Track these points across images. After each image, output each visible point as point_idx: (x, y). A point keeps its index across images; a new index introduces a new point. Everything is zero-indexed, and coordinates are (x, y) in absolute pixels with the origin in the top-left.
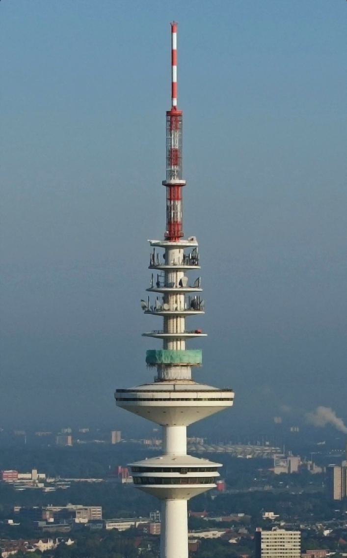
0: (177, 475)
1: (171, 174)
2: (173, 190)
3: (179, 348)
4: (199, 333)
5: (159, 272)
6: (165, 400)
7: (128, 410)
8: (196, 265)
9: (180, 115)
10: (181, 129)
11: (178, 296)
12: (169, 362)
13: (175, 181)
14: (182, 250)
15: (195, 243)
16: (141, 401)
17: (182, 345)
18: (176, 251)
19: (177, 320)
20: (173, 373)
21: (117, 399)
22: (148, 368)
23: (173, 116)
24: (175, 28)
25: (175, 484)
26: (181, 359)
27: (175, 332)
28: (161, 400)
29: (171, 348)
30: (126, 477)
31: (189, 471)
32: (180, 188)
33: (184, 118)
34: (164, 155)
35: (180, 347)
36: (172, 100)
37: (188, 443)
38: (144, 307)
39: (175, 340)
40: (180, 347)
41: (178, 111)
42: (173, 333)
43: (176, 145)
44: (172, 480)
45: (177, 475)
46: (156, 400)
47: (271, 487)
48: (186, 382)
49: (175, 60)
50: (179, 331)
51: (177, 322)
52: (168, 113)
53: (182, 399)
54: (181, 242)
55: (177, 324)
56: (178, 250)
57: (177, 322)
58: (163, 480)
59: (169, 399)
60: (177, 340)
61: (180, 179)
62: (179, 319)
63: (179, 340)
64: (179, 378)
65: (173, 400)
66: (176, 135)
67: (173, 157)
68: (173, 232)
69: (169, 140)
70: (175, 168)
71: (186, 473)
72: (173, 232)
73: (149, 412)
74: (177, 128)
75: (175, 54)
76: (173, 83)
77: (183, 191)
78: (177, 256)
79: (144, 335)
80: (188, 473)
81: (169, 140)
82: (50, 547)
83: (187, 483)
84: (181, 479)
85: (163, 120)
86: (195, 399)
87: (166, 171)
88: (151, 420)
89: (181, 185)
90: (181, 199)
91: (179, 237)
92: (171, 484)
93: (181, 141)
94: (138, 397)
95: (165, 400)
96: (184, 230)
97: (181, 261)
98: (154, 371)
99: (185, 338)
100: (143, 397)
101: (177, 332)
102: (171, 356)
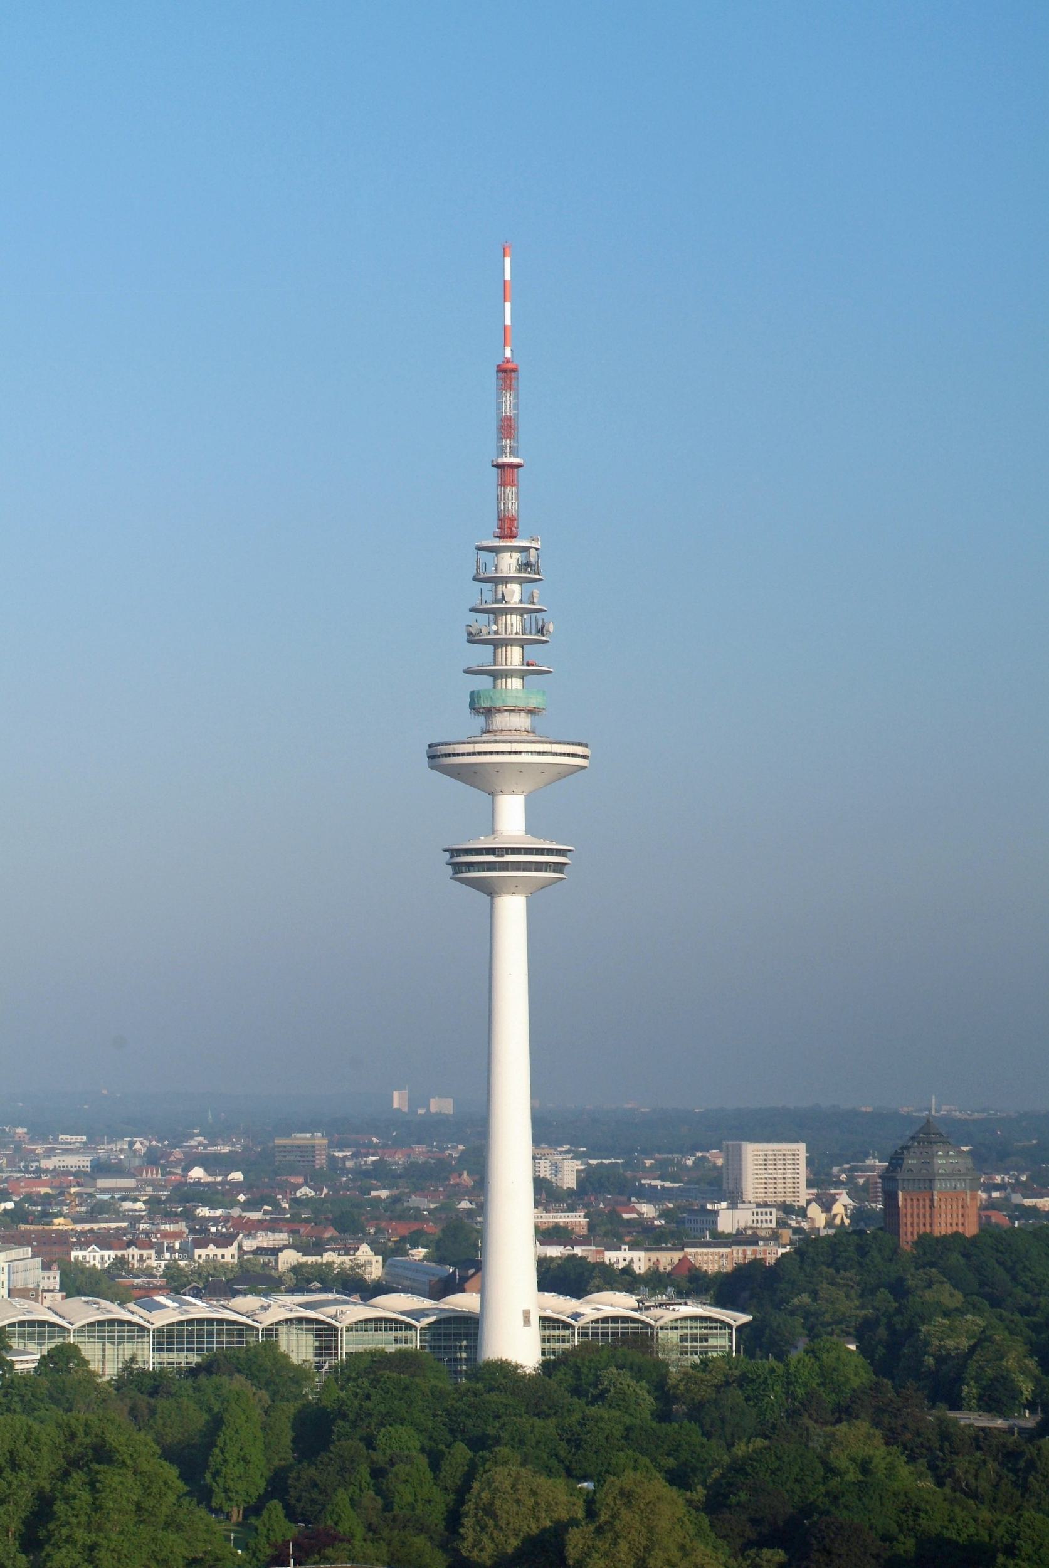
1: (502, 451)
3: (504, 687)
4: (533, 665)
5: (489, 586)
6: (469, 754)
7: (436, 770)
8: (529, 573)
9: (515, 370)
10: (516, 390)
11: (509, 616)
14: (516, 555)
17: (515, 683)
18: (506, 555)
20: (502, 721)
21: (429, 757)
22: (476, 717)
23: (506, 373)
24: (507, 250)
27: (504, 664)
28: (463, 754)
31: (507, 854)
38: (470, 634)
39: (504, 676)
41: (510, 365)
43: (508, 410)
44: (528, 865)
46: (459, 755)
48: (523, 733)
49: (508, 342)
50: (509, 664)
52: (501, 369)
54: (515, 543)
59: (474, 754)
60: (506, 677)
61: (516, 456)
62: (509, 648)
63: (504, 676)
64: (506, 729)
65: (479, 753)
66: (509, 398)
67: (507, 428)
68: (507, 528)
69: (499, 408)
71: (502, 856)
72: (507, 528)
78: (509, 563)
79: (468, 671)
81: (499, 408)
83: (518, 870)
86: (510, 753)
88: (476, 787)
89: (519, 466)
90: (515, 485)
91: (513, 537)
92: (508, 871)
95: (469, 754)
96: (521, 527)
97: (513, 569)
98: (481, 720)
99: (520, 612)
101: (506, 665)
102: (491, 698)
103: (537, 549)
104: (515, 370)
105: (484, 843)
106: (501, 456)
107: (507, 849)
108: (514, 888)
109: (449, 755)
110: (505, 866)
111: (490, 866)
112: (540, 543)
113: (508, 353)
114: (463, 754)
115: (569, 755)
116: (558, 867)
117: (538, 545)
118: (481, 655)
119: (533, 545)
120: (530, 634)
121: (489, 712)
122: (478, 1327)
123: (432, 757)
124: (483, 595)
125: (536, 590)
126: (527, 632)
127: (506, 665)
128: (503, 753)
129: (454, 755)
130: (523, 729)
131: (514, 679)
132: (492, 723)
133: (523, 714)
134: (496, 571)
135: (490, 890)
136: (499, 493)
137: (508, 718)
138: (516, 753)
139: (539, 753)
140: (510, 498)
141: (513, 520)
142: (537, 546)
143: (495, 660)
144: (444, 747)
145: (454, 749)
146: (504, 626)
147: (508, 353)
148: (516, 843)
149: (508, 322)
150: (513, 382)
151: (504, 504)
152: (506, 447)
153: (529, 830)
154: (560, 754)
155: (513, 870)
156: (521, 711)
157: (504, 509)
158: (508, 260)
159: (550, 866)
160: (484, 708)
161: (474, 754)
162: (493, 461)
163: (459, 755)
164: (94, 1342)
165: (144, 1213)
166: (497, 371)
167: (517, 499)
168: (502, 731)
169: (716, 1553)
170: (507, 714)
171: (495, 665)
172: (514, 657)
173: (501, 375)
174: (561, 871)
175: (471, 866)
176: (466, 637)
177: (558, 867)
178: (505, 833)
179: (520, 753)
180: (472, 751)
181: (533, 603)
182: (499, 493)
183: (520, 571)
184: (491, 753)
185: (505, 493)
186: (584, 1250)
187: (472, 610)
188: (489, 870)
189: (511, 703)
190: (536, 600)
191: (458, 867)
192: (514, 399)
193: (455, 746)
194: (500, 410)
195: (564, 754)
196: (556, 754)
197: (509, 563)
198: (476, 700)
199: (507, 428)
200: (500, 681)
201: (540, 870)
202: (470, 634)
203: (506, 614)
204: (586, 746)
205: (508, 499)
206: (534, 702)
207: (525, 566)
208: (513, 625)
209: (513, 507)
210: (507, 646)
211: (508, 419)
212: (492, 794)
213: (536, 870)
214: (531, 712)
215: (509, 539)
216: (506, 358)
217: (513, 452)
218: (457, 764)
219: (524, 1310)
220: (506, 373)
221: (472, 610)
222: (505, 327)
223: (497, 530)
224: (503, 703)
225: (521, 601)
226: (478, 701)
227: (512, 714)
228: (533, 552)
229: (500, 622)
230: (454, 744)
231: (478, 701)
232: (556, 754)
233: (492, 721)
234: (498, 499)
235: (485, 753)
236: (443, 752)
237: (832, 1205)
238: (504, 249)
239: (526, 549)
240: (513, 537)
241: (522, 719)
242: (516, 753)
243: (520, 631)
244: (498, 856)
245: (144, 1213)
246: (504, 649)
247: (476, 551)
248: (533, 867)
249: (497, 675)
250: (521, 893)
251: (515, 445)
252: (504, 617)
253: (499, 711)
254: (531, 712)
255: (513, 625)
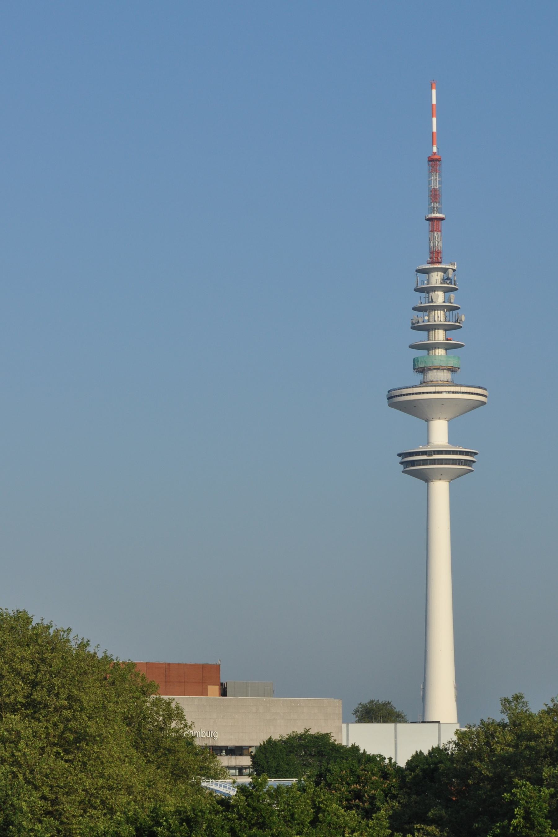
0: (425, 457)
1: (432, 211)
3: (434, 354)
4: (451, 340)
6: (410, 394)
12: (423, 366)
16: (393, 398)
17: (440, 352)
19: (435, 332)
20: (433, 375)
24: (434, 85)
25: (430, 464)
26: (432, 362)
27: (433, 340)
28: (407, 395)
29: (431, 354)
31: (435, 454)
32: (440, 222)
33: (443, 162)
34: (426, 196)
35: (435, 353)
36: (432, 147)
40: (435, 353)
41: (436, 157)
42: (432, 340)
45: (425, 457)
46: (404, 395)
49: (435, 142)
51: (435, 333)
53: (427, 393)
55: (435, 335)
56: (436, 273)
57: (435, 333)
58: (429, 462)
59: (413, 394)
63: (434, 348)
65: (416, 394)
66: (436, 177)
67: (434, 195)
70: (434, 205)
71: (431, 455)
73: (415, 406)
74: (436, 171)
79: (413, 347)
80: (434, 456)
83: (442, 464)
84: (444, 460)
86: (435, 393)
87: (429, 208)
89: (442, 219)
90: (440, 231)
93: (440, 182)
94: (392, 395)
95: (410, 394)
96: (444, 256)
97: (439, 282)
100: (405, 393)
102: (425, 361)
103: (454, 270)
104: (439, 160)
105: (421, 449)
106: (431, 213)
107: (434, 451)
108: (440, 476)
109: (399, 396)
110: (433, 462)
111: (425, 462)
112: (456, 266)
113: (435, 149)
114: (407, 395)
115: (472, 393)
117: (455, 267)
118: (420, 337)
119: (451, 267)
120: (449, 321)
121: (423, 371)
122: (381, 722)
123: (389, 398)
124: (420, 300)
125: (452, 295)
126: (447, 320)
127: (435, 340)
128: (431, 393)
129: (401, 395)
130: (446, 380)
131: (439, 350)
132: (427, 377)
133: (445, 371)
134: (428, 283)
135: (426, 478)
136: (430, 236)
137: (436, 374)
138: (438, 392)
139: (453, 392)
140: (437, 239)
141: (438, 253)
142: (453, 268)
143: (428, 339)
144: (396, 391)
145: (401, 392)
146: (433, 317)
147: (435, 149)
148: (442, 448)
150: (438, 168)
151: (433, 242)
152: (434, 208)
153: (450, 442)
154: (466, 393)
155: (438, 464)
156: (443, 369)
157: (433, 245)
158: (434, 91)
159: (462, 462)
160: (421, 368)
161: (413, 394)
162: (426, 217)
163: (404, 395)
166: (429, 161)
167: (441, 240)
168: (432, 381)
169: (320, 761)
170: (435, 371)
171: (428, 341)
172: (440, 336)
173: (431, 163)
174: (469, 466)
175: (413, 463)
176: (410, 325)
178: (435, 444)
179: (441, 392)
180: (412, 392)
181: (451, 302)
182: (430, 236)
183: (442, 283)
184: (423, 393)
185: (433, 236)
187: (415, 309)
188: (424, 465)
189: (437, 363)
190: (452, 301)
191: (406, 464)
192: (439, 178)
193: (401, 390)
194: (430, 185)
195: (472, 393)
196: (463, 393)
197: (436, 279)
198: (416, 363)
199: (434, 195)
200: (431, 351)
201: (456, 464)
202: (413, 324)
203: (435, 310)
204: (485, 389)
205: (435, 240)
206: (452, 363)
207: (446, 280)
208: (439, 317)
209: (439, 244)
210: (435, 329)
211: (435, 190)
212: (427, 420)
213: (453, 464)
214: (452, 370)
215: (438, 264)
216: (434, 152)
218: (402, 401)
220: (434, 161)
221: (415, 309)
222: (433, 133)
223: (429, 259)
224: (432, 364)
225: (444, 302)
226: (417, 364)
227: (439, 371)
228: (450, 271)
229: (431, 315)
230: (401, 389)
231: (417, 364)
232: (463, 393)
233: (426, 376)
234: (429, 240)
235: (420, 393)
236: (395, 395)
238: (432, 84)
239: (445, 271)
240: (440, 263)
241: (445, 374)
242: (438, 392)
243: (444, 320)
244: (429, 456)
246: (433, 331)
247: (416, 273)
248: (451, 462)
249: (429, 347)
250: (444, 479)
251: (440, 206)
252: (433, 312)
253: (430, 369)
254: (452, 370)
255: (439, 317)
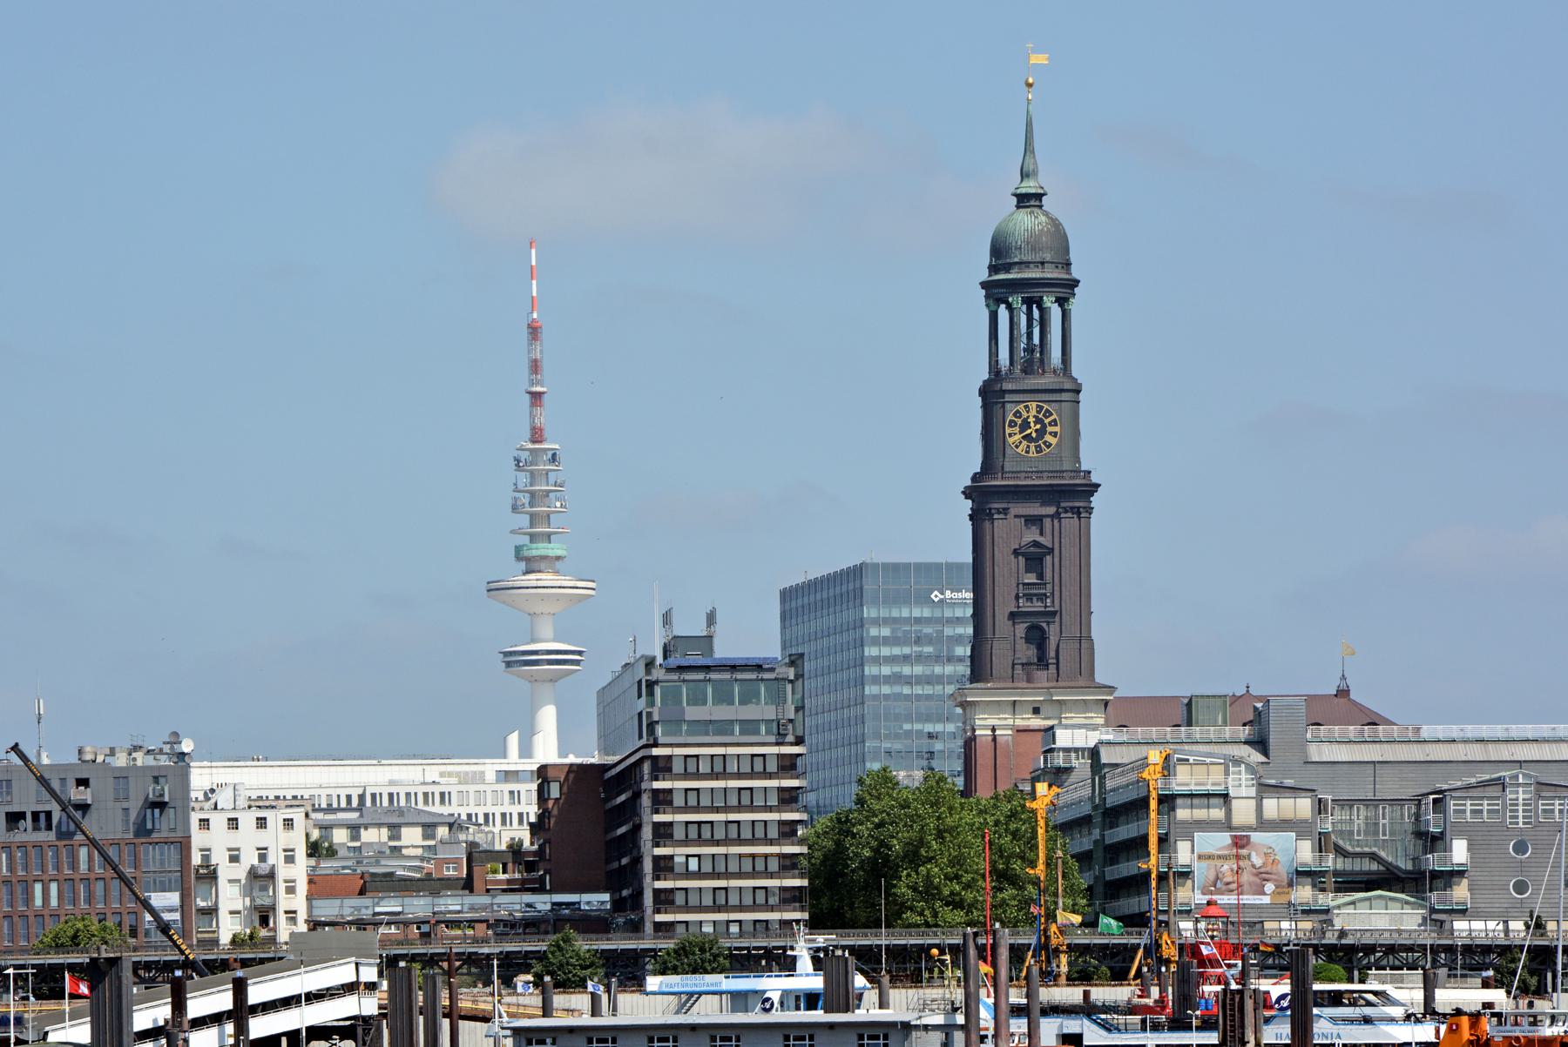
1: (532, 383)
2: (536, 397)
13: (538, 389)
15: (557, 447)
21: (488, 591)
23: (534, 331)
24: (533, 244)
30: (1278, 890)
37: (837, 1012)
47: (421, 1004)
49: (534, 275)
52: (529, 326)
67: (535, 367)
69: (532, 417)
75: (535, 271)
76: (532, 297)
77: (546, 398)
79: (513, 532)
82: (1028, 649)
85: (525, 331)
89: (544, 393)
93: (541, 351)
96: (546, 434)
116: (577, 662)
147: (535, 315)
149: (534, 263)
164: (300, 974)
165: (968, 601)
177: (577, 662)
186: (826, 940)
191: (509, 664)
199: (535, 367)
204: (594, 581)
211: (535, 361)
217: (538, 383)
219: (980, 283)
222: (532, 266)
237: (973, 525)
238: (531, 243)
245: (968, 601)
